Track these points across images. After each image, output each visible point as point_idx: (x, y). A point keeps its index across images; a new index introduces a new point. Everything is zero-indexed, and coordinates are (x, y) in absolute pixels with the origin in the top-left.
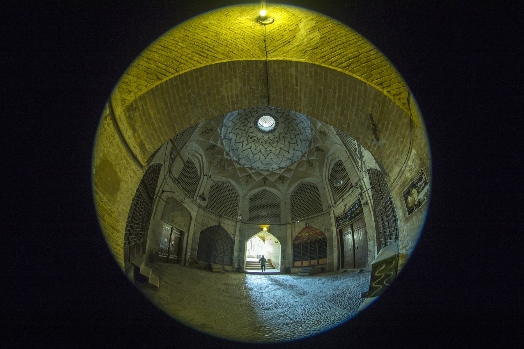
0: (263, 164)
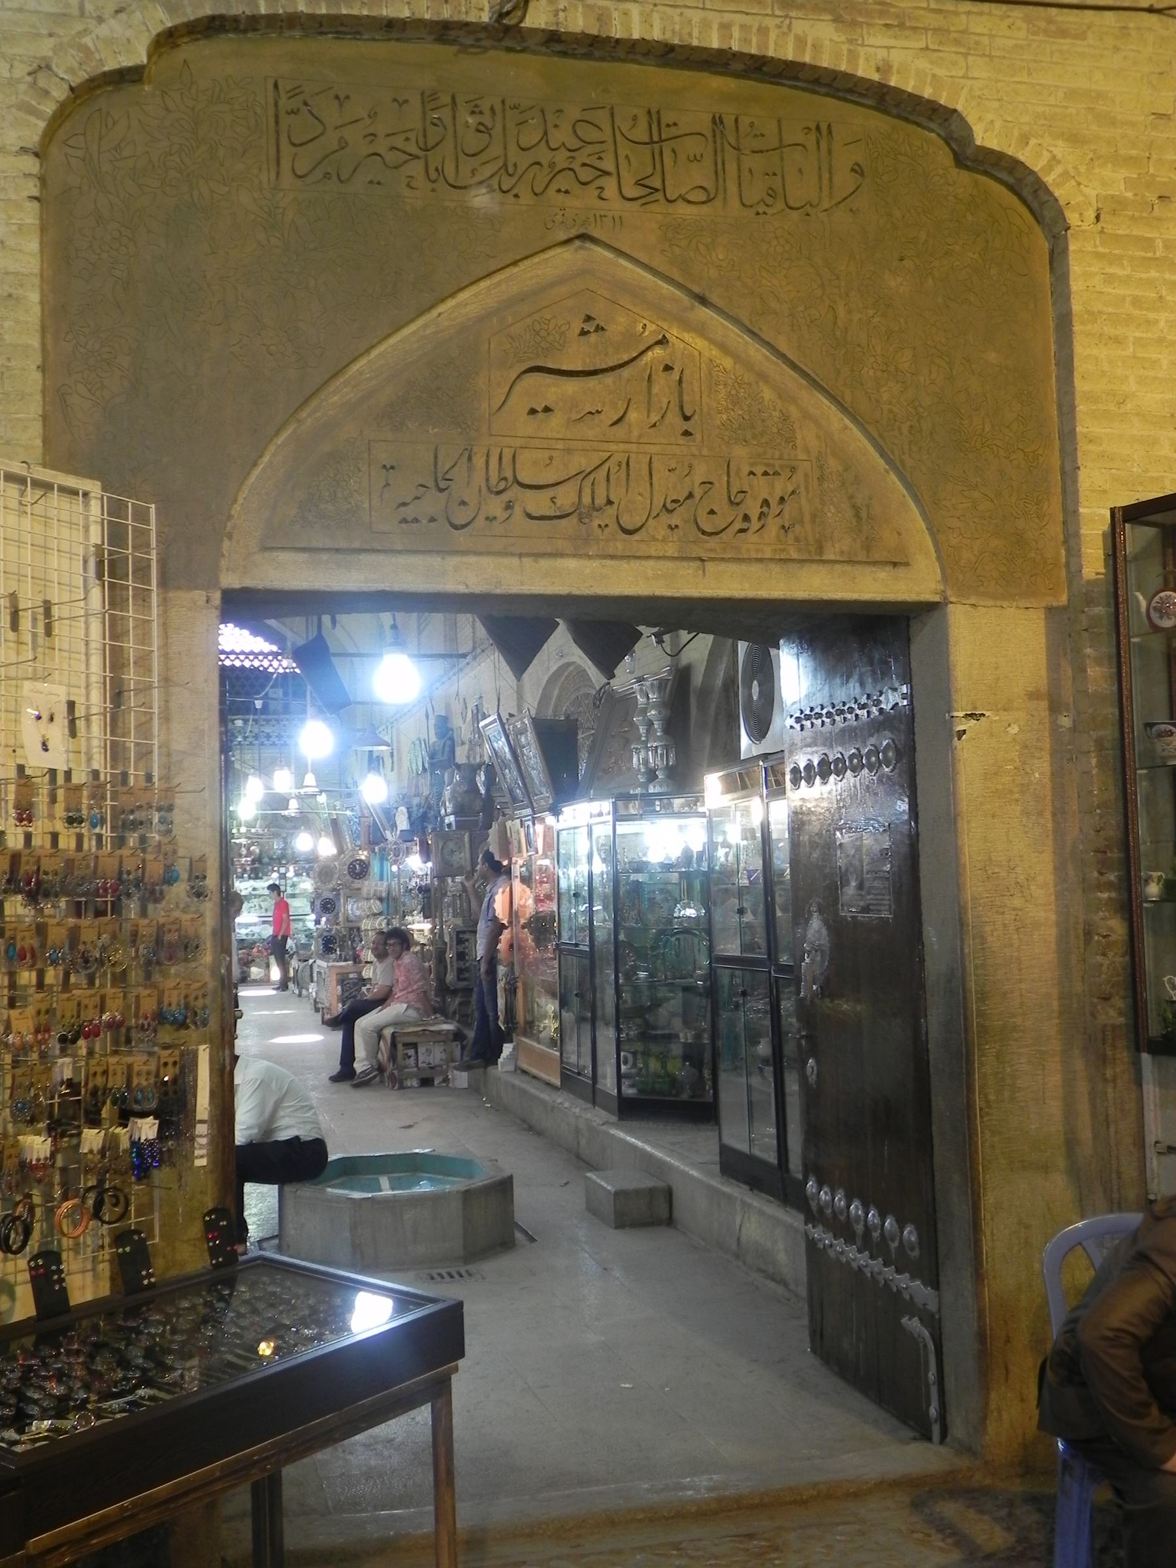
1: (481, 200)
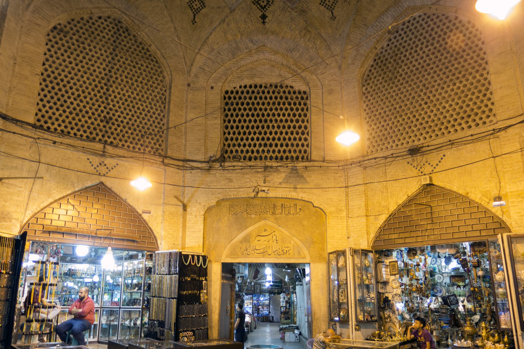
1: (253, 216)
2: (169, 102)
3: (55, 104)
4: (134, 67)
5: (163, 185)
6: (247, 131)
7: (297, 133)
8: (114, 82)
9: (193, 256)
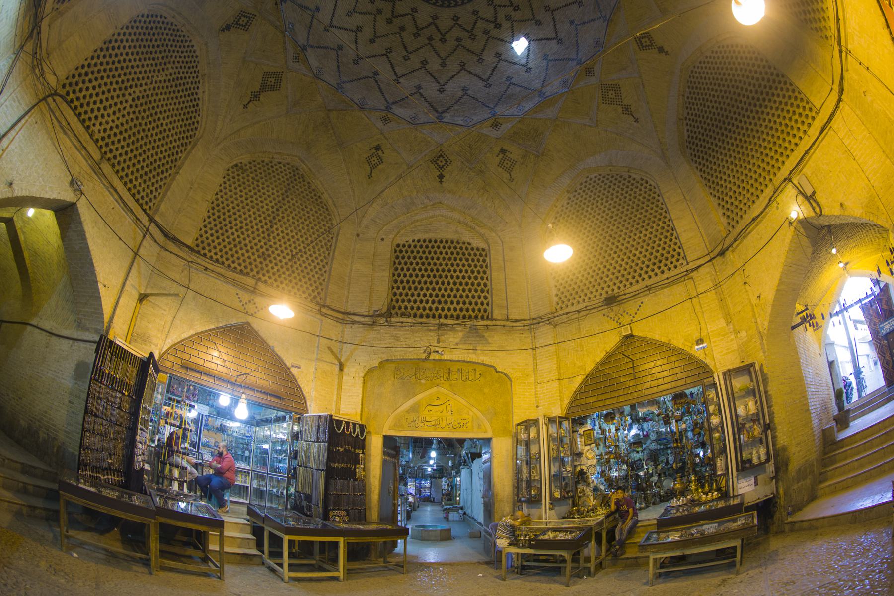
0: (593, 20)
1: (423, 381)
2: (335, 248)
3: (217, 232)
4: (303, 210)
5: (318, 338)
6: (419, 286)
7: (476, 291)
8: (279, 221)
9: (348, 423)
